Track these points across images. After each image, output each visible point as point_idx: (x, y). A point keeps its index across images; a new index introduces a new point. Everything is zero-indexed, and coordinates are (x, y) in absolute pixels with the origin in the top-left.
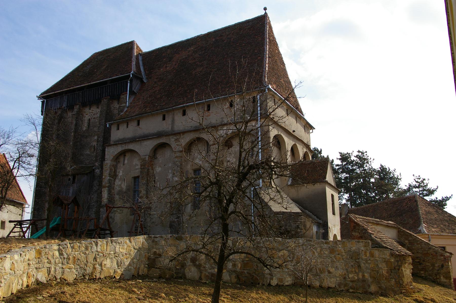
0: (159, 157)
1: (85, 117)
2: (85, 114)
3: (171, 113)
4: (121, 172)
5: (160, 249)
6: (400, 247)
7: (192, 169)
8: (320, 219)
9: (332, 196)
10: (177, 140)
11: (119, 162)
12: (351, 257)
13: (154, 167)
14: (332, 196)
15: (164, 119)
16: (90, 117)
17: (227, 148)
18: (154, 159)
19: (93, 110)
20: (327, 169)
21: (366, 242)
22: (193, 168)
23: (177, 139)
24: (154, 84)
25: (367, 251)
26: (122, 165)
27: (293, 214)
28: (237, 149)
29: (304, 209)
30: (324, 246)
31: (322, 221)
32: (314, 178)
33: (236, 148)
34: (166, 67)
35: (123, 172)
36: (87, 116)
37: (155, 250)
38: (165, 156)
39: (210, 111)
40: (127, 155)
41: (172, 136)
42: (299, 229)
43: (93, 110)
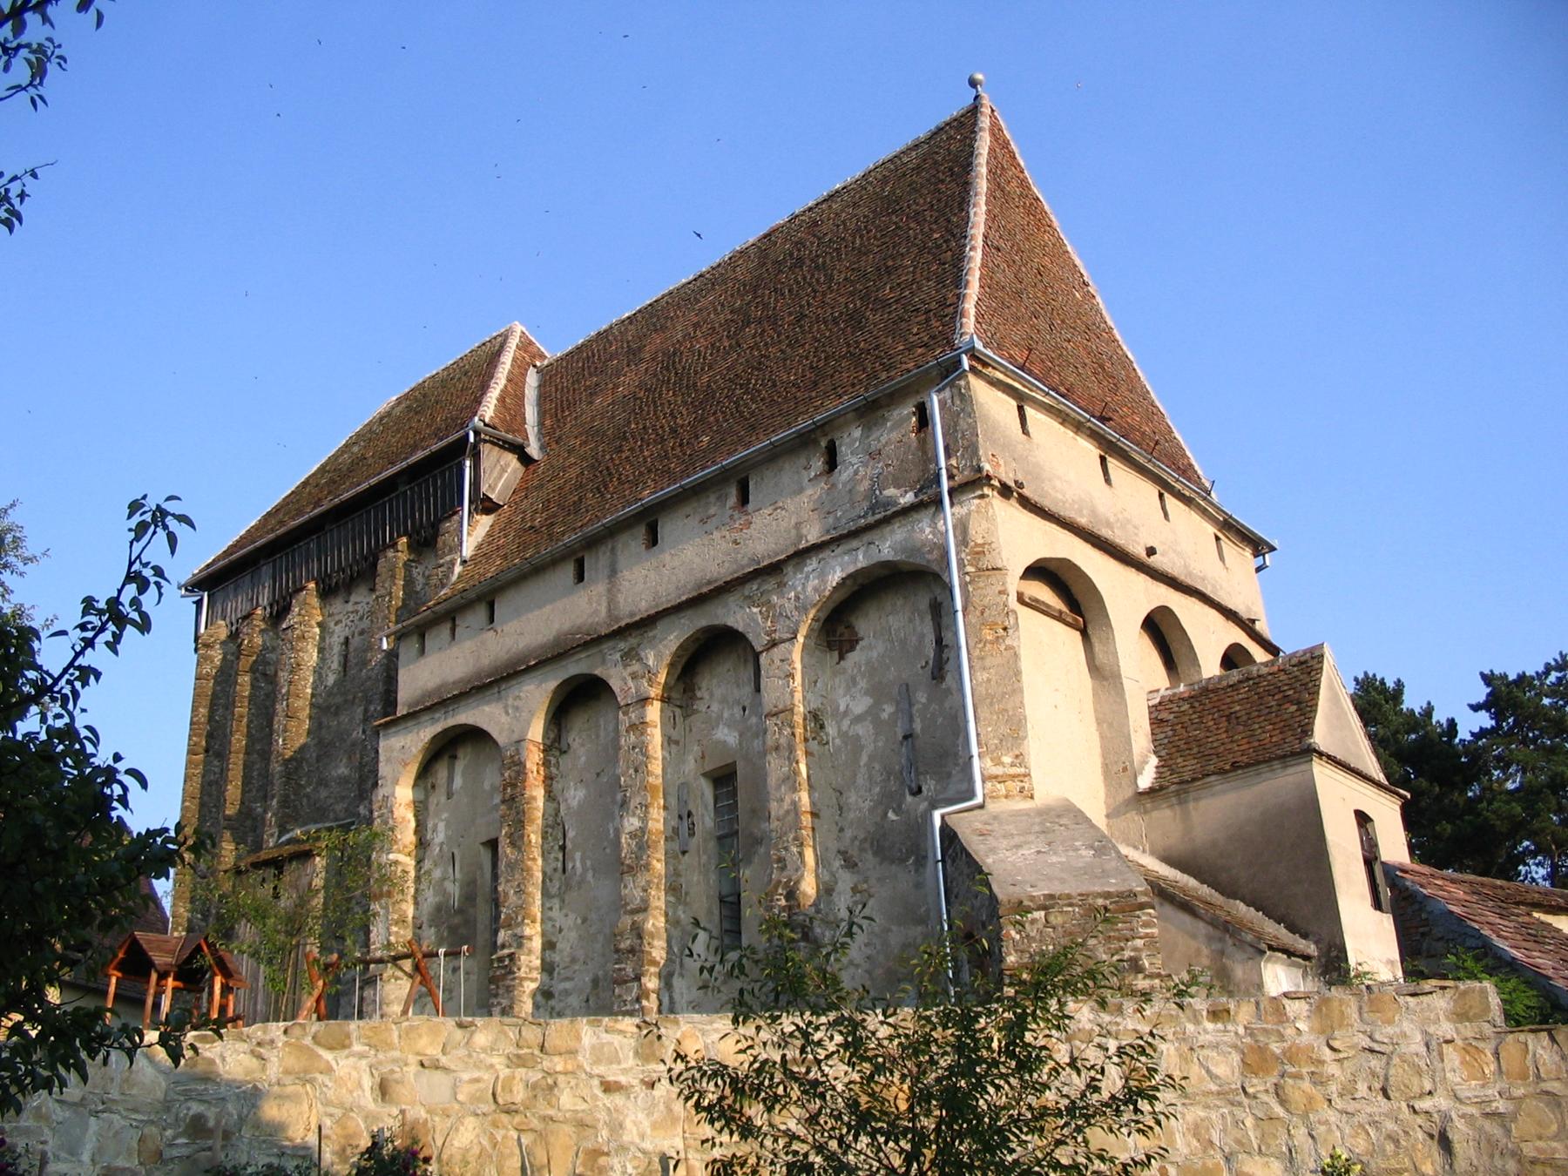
0: (575, 745)
1: (333, 632)
2: (332, 624)
3: (603, 548)
4: (441, 826)
5: (223, 1099)
6: (801, 639)
7: (705, 775)
8: (1305, 936)
9: (1363, 819)
10: (630, 655)
11: (433, 787)
12: (1377, 1086)
13: (560, 786)
14: (1363, 819)
15: (580, 577)
16: (347, 632)
17: (836, 654)
18: (557, 753)
19: (356, 603)
20: (1317, 693)
21: (1465, 993)
22: (707, 769)
23: (632, 649)
24: (565, 459)
25: (1481, 1045)
26: (443, 799)
27: (1100, 902)
28: (875, 654)
29: (1222, 893)
30: (1206, 1031)
31: (1316, 943)
32: (1256, 744)
33: (870, 647)
34: (616, 386)
35: (447, 827)
36: (338, 629)
37: (196, 1108)
38: (598, 736)
39: (750, 507)
40: (460, 753)
41: (611, 644)
42: (1140, 976)
43: (356, 603)
